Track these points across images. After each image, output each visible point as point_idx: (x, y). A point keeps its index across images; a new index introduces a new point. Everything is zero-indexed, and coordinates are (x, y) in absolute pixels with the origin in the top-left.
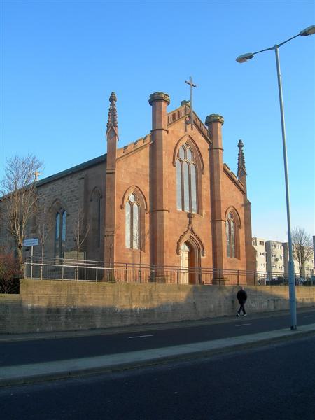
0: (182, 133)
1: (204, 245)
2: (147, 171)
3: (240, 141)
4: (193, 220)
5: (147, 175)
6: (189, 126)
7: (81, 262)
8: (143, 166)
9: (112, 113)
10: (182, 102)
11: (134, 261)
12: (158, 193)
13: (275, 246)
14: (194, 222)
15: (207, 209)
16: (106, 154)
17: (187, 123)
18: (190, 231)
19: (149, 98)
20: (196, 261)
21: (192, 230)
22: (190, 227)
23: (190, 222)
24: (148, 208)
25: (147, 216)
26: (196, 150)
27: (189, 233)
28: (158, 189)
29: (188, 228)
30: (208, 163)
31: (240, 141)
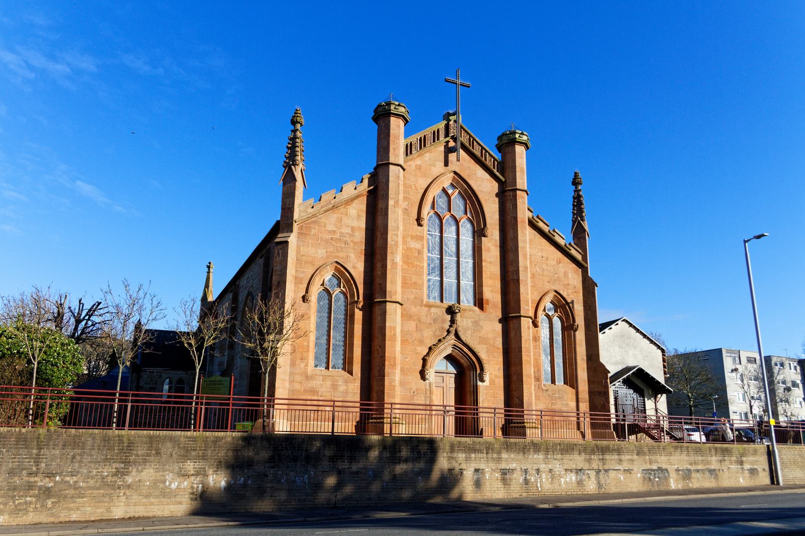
0: (440, 167)
1: (484, 362)
2: (360, 236)
3: (576, 174)
4: (458, 317)
5: (392, 198)
6: (452, 157)
7: (473, 373)
8: (353, 228)
9: (294, 139)
10: (304, 301)
11: (431, 400)
12: (379, 272)
13: (782, 365)
14: (462, 321)
15: (492, 291)
16: (279, 221)
17: (448, 150)
18: (452, 336)
19: (373, 114)
20: (469, 389)
21: (457, 336)
22: (453, 330)
23: (453, 321)
24: (361, 298)
25: (359, 315)
26: (471, 197)
27: (451, 339)
28: (379, 265)
29: (449, 332)
30: (497, 216)
31: (576, 174)
